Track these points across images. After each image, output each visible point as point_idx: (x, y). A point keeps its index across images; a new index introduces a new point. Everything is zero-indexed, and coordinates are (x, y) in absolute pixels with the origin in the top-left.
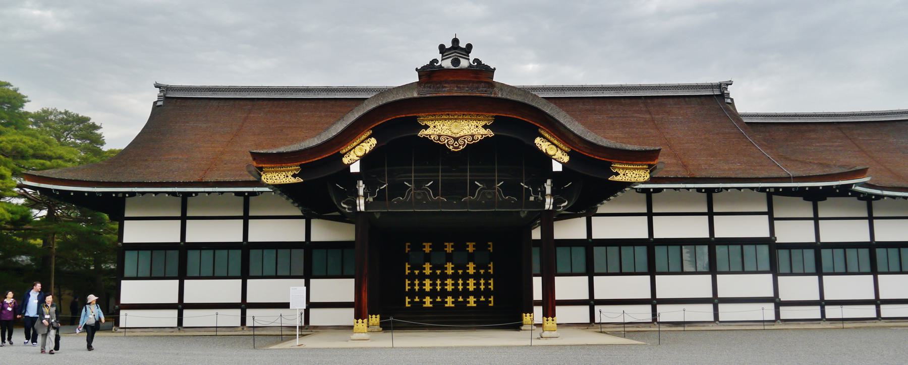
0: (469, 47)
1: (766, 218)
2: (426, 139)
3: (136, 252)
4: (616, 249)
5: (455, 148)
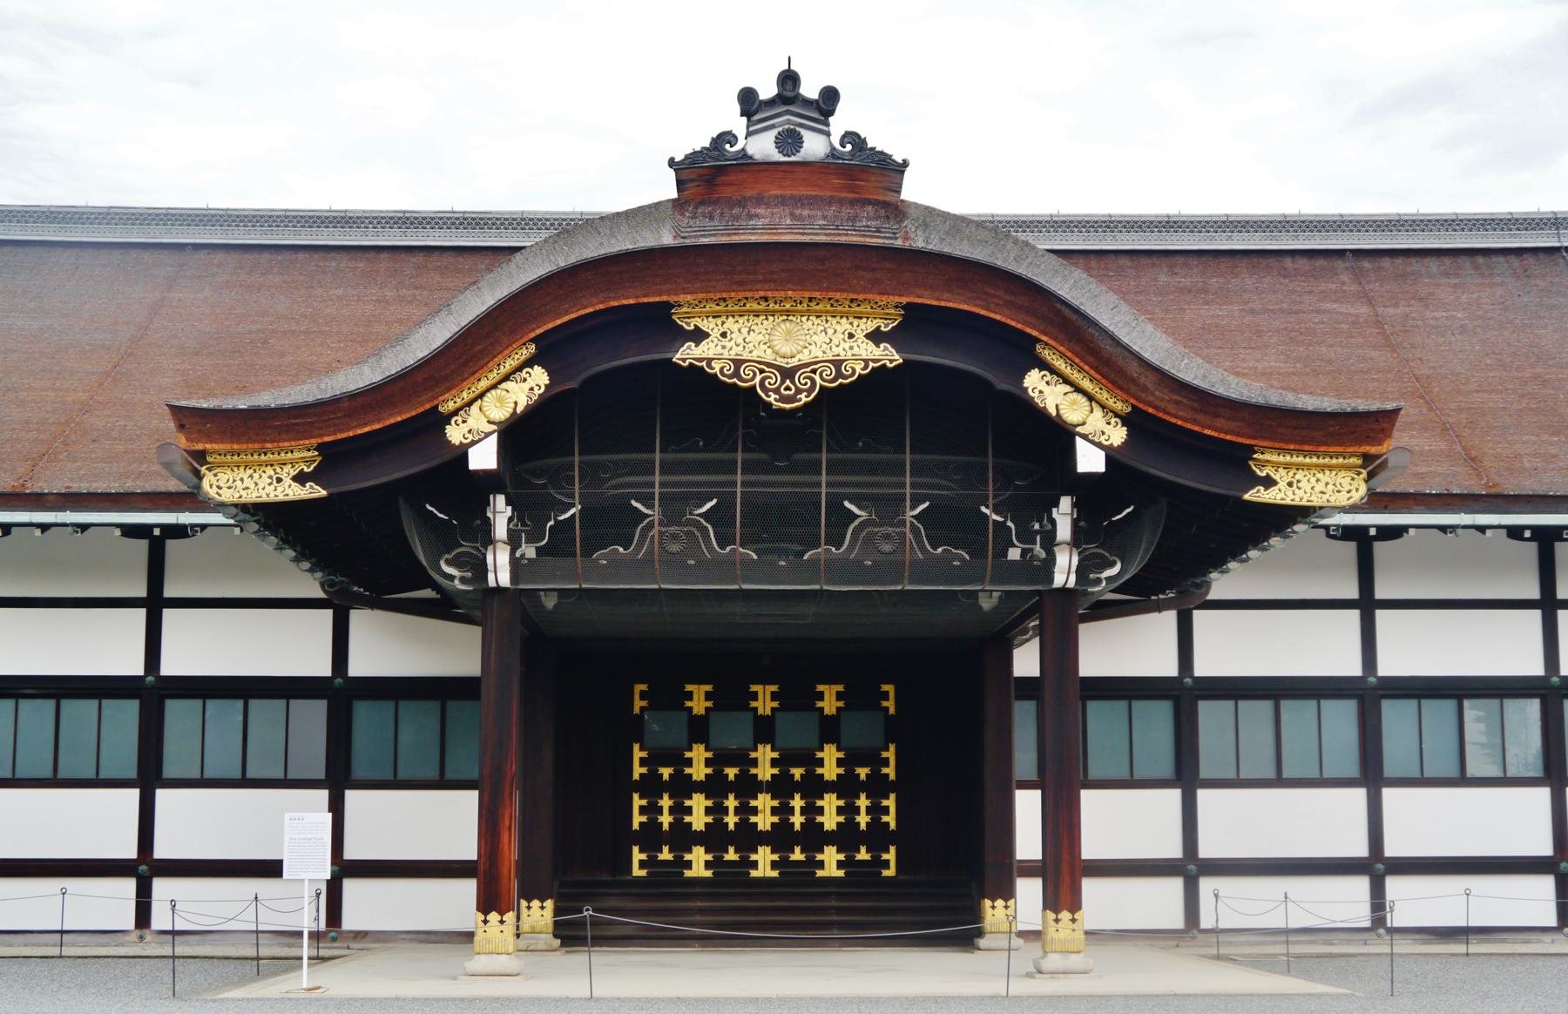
0: (830, 97)
2: (697, 374)
5: (810, 391)
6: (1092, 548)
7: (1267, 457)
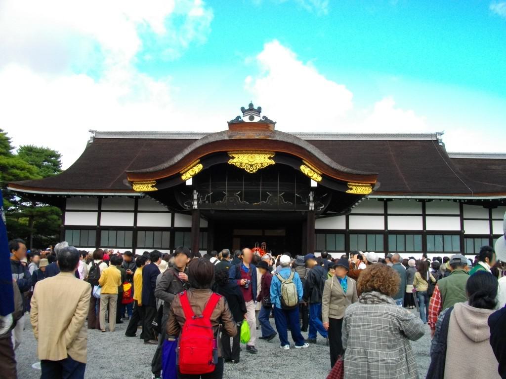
0: (260, 108)
1: (459, 218)
2: (233, 166)
3: (79, 231)
4: (364, 236)
5: (256, 169)
6: (318, 202)
7: (351, 184)
